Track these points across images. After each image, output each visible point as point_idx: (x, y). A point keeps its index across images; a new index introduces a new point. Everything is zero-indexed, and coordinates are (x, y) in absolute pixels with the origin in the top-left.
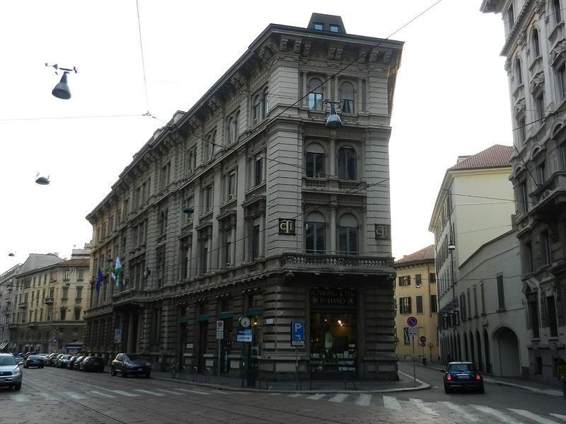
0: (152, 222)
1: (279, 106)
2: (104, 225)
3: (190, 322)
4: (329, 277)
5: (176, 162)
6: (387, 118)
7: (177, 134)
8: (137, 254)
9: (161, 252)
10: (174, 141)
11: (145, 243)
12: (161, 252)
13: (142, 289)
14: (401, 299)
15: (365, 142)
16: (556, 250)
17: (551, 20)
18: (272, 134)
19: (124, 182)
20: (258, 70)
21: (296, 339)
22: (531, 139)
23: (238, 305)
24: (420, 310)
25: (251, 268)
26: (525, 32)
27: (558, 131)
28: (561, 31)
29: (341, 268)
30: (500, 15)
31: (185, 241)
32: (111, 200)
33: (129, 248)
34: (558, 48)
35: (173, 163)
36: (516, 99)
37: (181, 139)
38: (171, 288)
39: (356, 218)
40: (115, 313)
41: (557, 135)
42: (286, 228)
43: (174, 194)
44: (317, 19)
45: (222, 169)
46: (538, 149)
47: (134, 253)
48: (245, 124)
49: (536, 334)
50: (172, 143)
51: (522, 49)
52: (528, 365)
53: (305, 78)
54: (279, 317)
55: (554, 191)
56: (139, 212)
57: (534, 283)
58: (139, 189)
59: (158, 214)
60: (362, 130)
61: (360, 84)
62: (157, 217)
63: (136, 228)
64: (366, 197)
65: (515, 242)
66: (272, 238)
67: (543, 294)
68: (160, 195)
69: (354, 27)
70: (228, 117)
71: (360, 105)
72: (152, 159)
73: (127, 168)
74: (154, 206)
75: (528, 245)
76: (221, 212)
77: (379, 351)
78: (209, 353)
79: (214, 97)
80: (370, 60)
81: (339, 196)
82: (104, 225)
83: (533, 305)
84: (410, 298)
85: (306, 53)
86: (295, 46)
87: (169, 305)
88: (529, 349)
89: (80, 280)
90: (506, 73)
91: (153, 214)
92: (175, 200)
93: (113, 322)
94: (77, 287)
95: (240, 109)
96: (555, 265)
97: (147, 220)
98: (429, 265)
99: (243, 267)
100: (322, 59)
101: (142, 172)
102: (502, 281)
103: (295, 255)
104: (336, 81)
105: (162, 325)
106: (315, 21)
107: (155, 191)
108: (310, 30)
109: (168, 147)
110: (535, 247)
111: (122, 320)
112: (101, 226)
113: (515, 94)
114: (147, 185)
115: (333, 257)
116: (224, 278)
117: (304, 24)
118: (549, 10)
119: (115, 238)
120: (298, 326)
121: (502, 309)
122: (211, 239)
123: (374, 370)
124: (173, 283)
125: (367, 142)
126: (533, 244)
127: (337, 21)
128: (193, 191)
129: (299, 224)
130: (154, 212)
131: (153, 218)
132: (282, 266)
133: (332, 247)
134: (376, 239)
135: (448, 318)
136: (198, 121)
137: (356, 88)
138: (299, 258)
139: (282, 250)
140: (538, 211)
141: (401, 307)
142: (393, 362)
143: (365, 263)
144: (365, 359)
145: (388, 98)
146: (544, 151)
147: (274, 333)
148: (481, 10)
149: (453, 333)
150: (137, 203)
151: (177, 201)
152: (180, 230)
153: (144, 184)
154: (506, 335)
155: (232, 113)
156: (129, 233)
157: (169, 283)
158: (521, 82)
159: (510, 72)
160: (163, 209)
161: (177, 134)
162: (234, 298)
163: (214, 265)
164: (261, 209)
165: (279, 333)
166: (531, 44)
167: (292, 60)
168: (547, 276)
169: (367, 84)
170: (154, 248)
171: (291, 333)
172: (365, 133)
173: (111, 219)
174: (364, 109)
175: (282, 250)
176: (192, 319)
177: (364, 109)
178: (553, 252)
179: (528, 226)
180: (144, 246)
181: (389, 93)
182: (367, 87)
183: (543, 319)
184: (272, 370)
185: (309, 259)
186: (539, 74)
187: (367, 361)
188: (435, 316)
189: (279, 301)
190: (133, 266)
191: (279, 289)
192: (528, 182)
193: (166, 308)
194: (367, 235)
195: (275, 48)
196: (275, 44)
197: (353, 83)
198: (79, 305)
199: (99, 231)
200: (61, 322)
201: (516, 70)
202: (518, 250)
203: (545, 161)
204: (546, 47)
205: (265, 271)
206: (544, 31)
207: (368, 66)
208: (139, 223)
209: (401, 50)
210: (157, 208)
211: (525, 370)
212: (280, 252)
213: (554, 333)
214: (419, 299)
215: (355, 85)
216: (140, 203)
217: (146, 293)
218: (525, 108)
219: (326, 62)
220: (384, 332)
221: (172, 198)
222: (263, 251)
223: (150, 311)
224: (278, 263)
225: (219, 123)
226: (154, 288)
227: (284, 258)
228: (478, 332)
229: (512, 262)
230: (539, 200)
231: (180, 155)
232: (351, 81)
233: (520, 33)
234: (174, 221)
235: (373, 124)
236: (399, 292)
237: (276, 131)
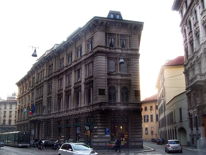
1: (98, 46)
3: (63, 127)
5: (55, 64)
6: (138, 50)
8: (39, 100)
11: (42, 95)
12: (49, 100)
13: (41, 114)
15: (130, 59)
16: (198, 100)
19: (32, 70)
21: (107, 134)
22: (202, 44)
26: (192, 10)
28: (198, 24)
30: (178, 12)
32: (26, 77)
34: (204, 19)
39: (125, 37)
40: (29, 123)
41: (186, 72)
42: (102, 92)
43: (55, 76)
44: (111, 13)
47: (37, 99)
48: (84, 51)
49: (192, 130)
51: (197, 6)
52: (189, 141)
54: (99, 126)
55: (196, 80)
57: (191, 112)
58: (39, 73)
59: (48, 84)
61: (128, 37)
62: (47, 85)
64: (131, 80)
65: (185, 96)
67: (194, 115)
68: (49, 76)
69: (126, 17)
71: (128, 45)
72: (45, 62)
73: (34, 65)
75: (189, 98)
76: (75, 85)
77: (136, 137)
78: (71, 139)
79: (72, 40)
80: (132, 28)
81: (121, 80)
82: (23, 87)
83: (191, 119)
84: (148, 116)
86: (104, 24)
87: (53, 120)
88: (190, 135)
89: (5, 108)
90: (181, 33)
91: (45, 84)
92: (55, 79)
94: (10, 111)
95: (82, 45)
96: (197, 105)
97: (43, 86)
98: (156, 102)
100: (114, 28)
105: (51, 128)
107: (46, 75)
108: (109, 18)
111: (33, 126)
112: (22, 87)
113: (185, 42)
114: (43, 72)
115: (119, 103)
116: (76, 111)
117: (105, 15)
118: (200, 4)
119: (28, 93)
120: (107, 129)
121: (181, 120)
122: (71, 95)
123: (134, 144)
126: (191, 97)
127: (119, 14)
128: (63, 76)
130: (46, 83)
132: (100, 107)
134: (135, 96)
137: (127, 39)
139: (100, 101)
142: (142, 141)
143: (131, 105)
144: (131, 141)
146: (194, 64)
147: (97, 132)
148: (172, 9)
149: (164, 129)
150: (38, 79)
151: (56, 79)
152: (57, 91)
153: (41, 72)
155: (89, 39)
156: (35, 91)
158: (197, 20)
165: (99, 132)
167: (103, 29)
168: (195, 109)
169: (131, 37)
171: (105, 132)
172: (130, 56)
173: (26, 85)
175: (100, 101)
176: (63, 126)
177: (130, 47)
178: (197, 101)
179: (189, 91)
180: (42, 97)
181: (139, 39)
182: (131, 38)
184: (97, 145)
186: (192, 36)
187: (132, 141)
188: (158, 123)
189: (99, 120)
190: (37, 105)
192: (202, 63)
193: (52, 122)
194: (132, 94)
196: (96, 24)
198: (11, 119)
201: (189, 24)
202: (186, 99)
205: (94, 108)
207: (131, 30)
211: (188, 143)
212: (99, 101)
213: (197, 129)
214: (152, 116)
215: (126, 38)
216: (40, 79)
217: (43, 115)
219: (115, 29)
220: (138, 130)
221: (54, 78)
225: (73, 50)
226: (47, 114)
227: (101, 104)
228: (169, 130)
230: (192, 83)
231: (57, 61)
232: (124, 36)
234: (55, 87)
235: (133, 52)
237: (97, 55)
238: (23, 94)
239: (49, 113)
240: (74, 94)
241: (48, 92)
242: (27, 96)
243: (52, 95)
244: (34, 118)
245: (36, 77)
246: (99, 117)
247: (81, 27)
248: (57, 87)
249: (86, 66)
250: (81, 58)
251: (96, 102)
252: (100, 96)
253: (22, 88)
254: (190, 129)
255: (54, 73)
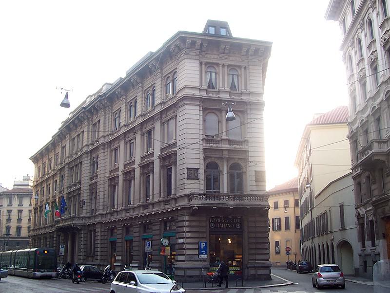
0: (86, 165)
2: (44, 164)
4: (223, 210)
5: (105, 121)
7: (105, 100)
8: (73, 188)
9: (93, 189)
10: (103, 105)
11: (80, 180)
12: (93, 189)
13: (79, 215)
14: (273, 219)
15: (247, 112)
16: (375, 189)
17: (368, 35)
18: (180, 107)
19: (61, 133)
20: (169, 59)
21: (202, 253)
22: (383, 83)
23: (157, 229)
24: (287, 228)
25: (165, 202)
26: (363, 20)
27: (374, 110)
28: (374, 44)
29: (232, 203)
31: (113, 181)
33: (66, 183)
34: (387, 35)
35: (102, 122)
36: (369, 51)
37: (109, 104)
38: (102, 215)
40: (56, 233)
41: (353, 135)
42: (192, 174)
43: (103, 145)
44: (211, 24)
45: (141, 128)
46: (375, 107)
47: (71, 187)
49: (364, 245)
50: (102, 107)
52: (358, 267)
53: (203, 66)
56: (74, 157)
57: (362, 211)
58: (74, 138)
59: (91, 159)
60: (245, 103)
61: (243, 70)
62: (89, 161)
63: (72, 168)
64: (248, 151)
65: (350, 182)
66: (182, 182)
68: (92, 144)
70: (146, 90)
72: (85, 118)
73: (65, 123)
74: (86, 153)
76: (142, 161)
77: (258, 260)
80: (250, 53)
81: (229, 151)
82: (44, 164)
83: (362, 225)
84: (280, 219)
85: (204, 49)
86: (196, 45)
88: (359, 255)
89: (10, 205)
91: (86, 159)
92: (104, 149)
93: (55, 239)
97: (81, 163)
98: (295, 193)
99: (160, 202)
100: (216, 53)
101: (76, 126)
102: (343, 209)
103: (199, 194)
104: (226, 68)
106: (209, 25)
107: (88, 141)
109: (98, 109)
110: (363, 186)
111: (63, 238)
112: (41, 165)
114: (81, 136)
115: (225, 195)
117: (200, 29)
118: (379, 8)
119: (54, 176)
120: (203, 245)
121: (343, 228)
122: (134, 180)
123: (255, 273)
124: (104, 211)
125: (249, 112)
127: (224, 26)
129: (201, 172)
130: (87, 157)
131: (86, 163)
132: (189, 201)
133: (225, 188)
134: (256, 182)
135: (308, 233)
136: (122, 91)
138: (201, 196)
139: (190, 190)
140: (363, 164)
141: (273, 226)
142: (268, 267)
144: (248, 266)
145: (263, 76)
147: (184, 249)
148: (325, 17)
149: (311, 245)
150: (73, 149)
151: (106, 150)
152: (108, 172)
153: (78, 135)
154: (345, 245)
157: (101, 212)
158: (373, 37)
159: (346, 62)
160: (94, 155)
161: (105, 100)
162: (153, 224)
163: (137, 197)
164: (172, 160)
166: (380, 7)
167: (194, 54)
168: (370, 207)
169: (247, 70)
170: (88, 185)
173: (50, 160)
174: (246, 88)
178: (373, 190)
179: (359, 172)
180: (80, 183)
182: (247, 73)
183: (367, 235)
184: (183, 275)
185: (208, 197)
187: (250, 267)
188: (299, 232)
189: (187, 226)
190: (70, 198)
191: (187, 218)
195: (182, 46)
196: (182, 45)
197: (238, 70)
198: (20, 225)
199: (39, 169)
200: (17, 238)
202: (353, 187)
203: (368, 128)
204: (378, 34)
205: (177, 205)
206: (377, 22)
207: (248, 57)
208: (75, 165)
209: (271, 47)
210: (90, 154)
211: (357, 270)
212: (187, 192)
213: (373, 245)
214: (287, 219)
216: (75, 149)
217: (82, 218)
218: (377, 58)
220: (261, 246)
221: (102, 147)
222: (175, 191)
223: (86, 231)
224: (186, 200)
226: (88, 215)
227: (190, 196)
229: (349, 196)
230: (363, 156)
231: (108, 115)
232: (235, 68)
233: (361, 20)
236: (272, 214)
237: (184, 105)
238: (43, 178)
239: (92, 215)
240: (140, 178)
241: (91, 174)
242: (52, 181)
243: (98, 180)
244: (65, 224)
245: (68, 146)
246: (187, 221)
247: (154, 50)
248: (108, 164)
249: (127, 145)
250: (154, 109)
251: (182, 192)
252: (190, 181)
253: (41, 166)
254: (359, 243)
255: (102, 139)
